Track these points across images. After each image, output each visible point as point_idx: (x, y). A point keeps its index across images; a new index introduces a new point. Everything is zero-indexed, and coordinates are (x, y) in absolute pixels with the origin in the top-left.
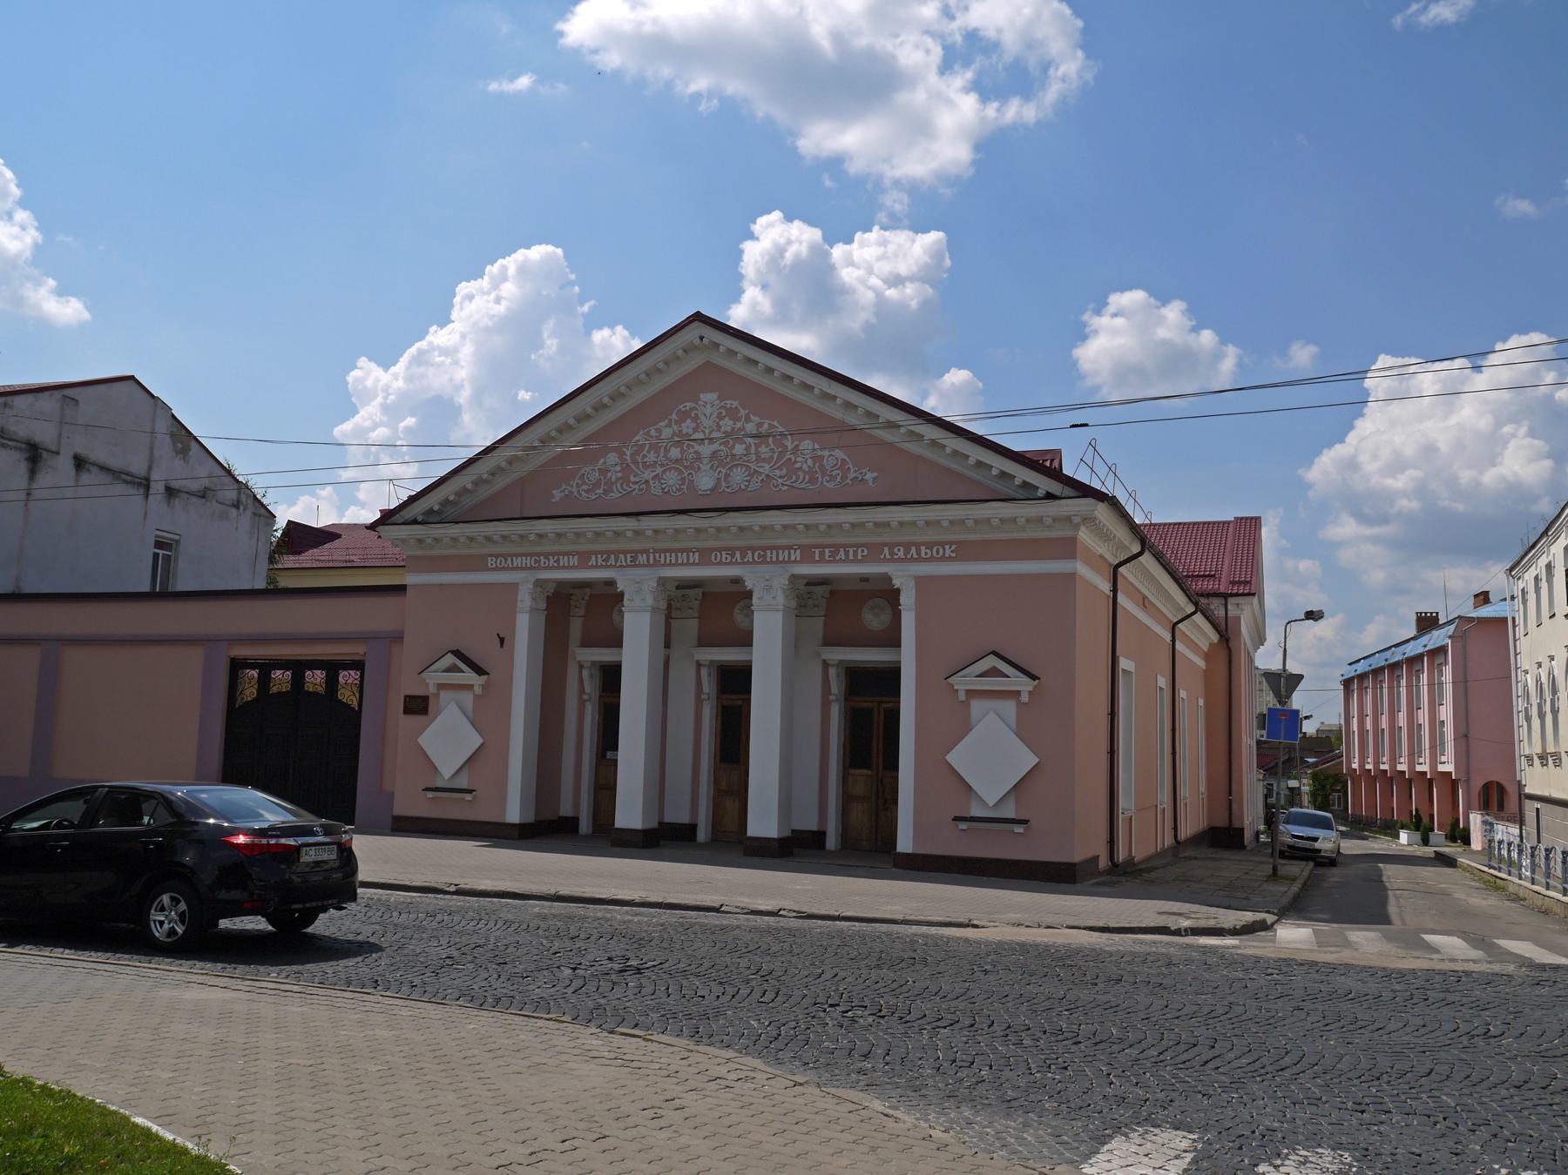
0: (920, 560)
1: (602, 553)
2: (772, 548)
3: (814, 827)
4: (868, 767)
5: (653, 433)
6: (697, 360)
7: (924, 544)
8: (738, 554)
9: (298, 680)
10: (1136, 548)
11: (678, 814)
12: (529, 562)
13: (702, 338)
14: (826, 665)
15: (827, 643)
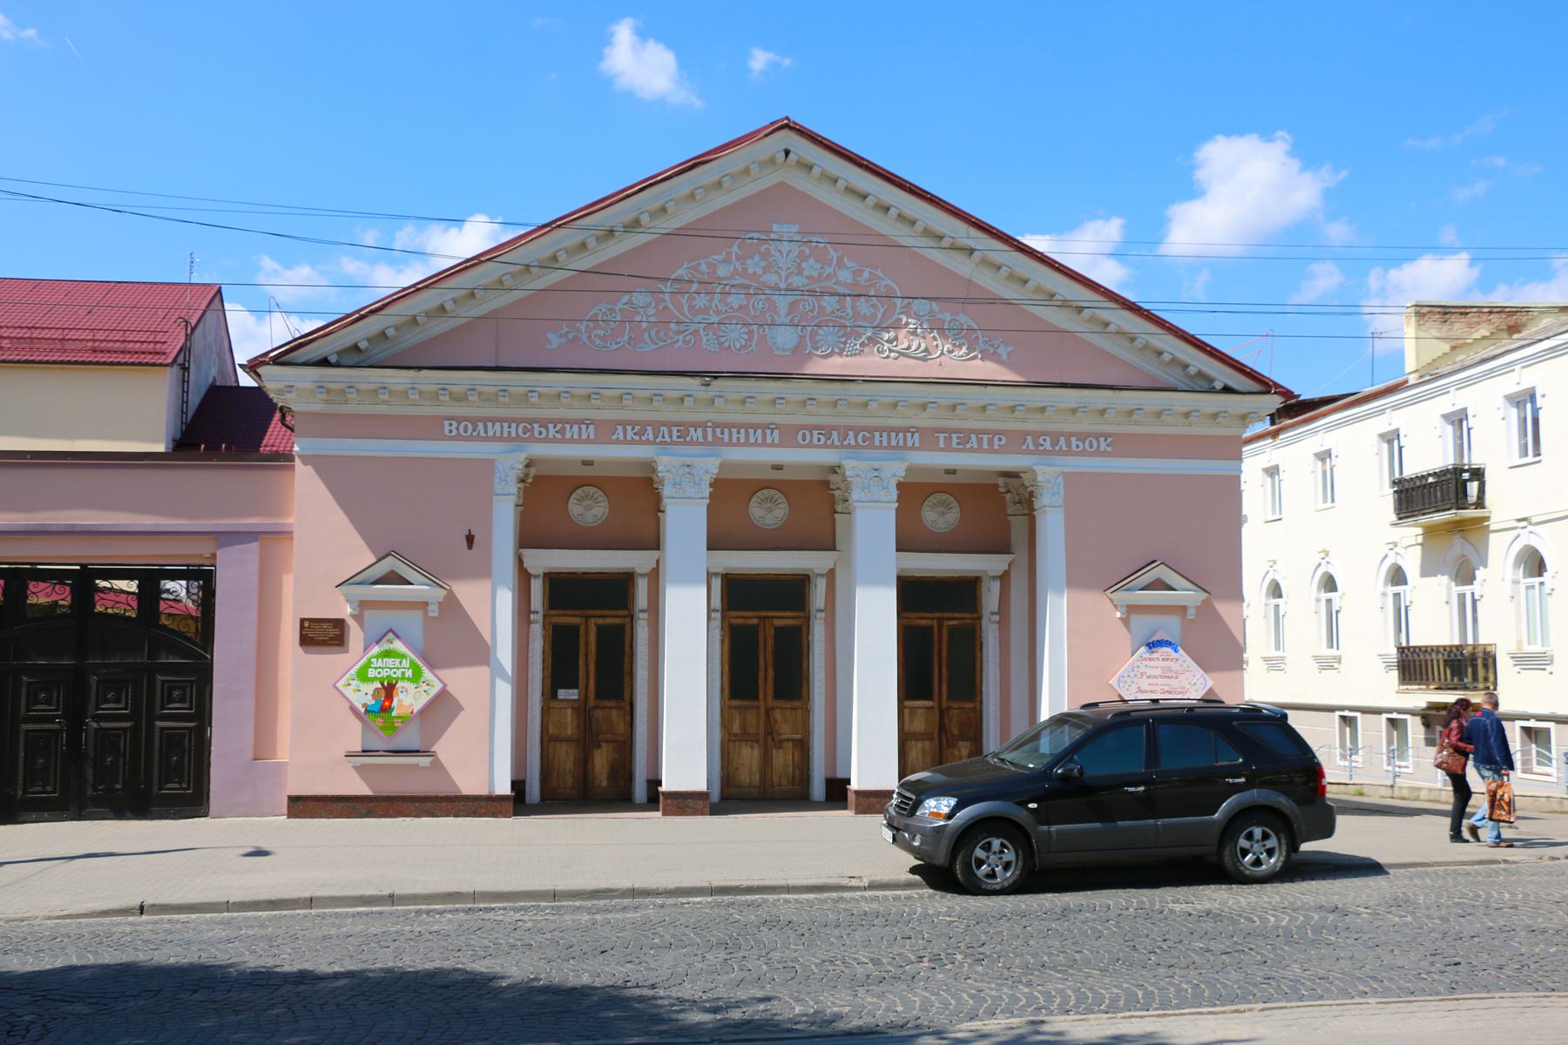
0: (1070, 453)
1: (633, 424)
2: (881, 430)
4: (928, 697)
5: (704, 268)
7: (1072, 434)
13: (787, 153)
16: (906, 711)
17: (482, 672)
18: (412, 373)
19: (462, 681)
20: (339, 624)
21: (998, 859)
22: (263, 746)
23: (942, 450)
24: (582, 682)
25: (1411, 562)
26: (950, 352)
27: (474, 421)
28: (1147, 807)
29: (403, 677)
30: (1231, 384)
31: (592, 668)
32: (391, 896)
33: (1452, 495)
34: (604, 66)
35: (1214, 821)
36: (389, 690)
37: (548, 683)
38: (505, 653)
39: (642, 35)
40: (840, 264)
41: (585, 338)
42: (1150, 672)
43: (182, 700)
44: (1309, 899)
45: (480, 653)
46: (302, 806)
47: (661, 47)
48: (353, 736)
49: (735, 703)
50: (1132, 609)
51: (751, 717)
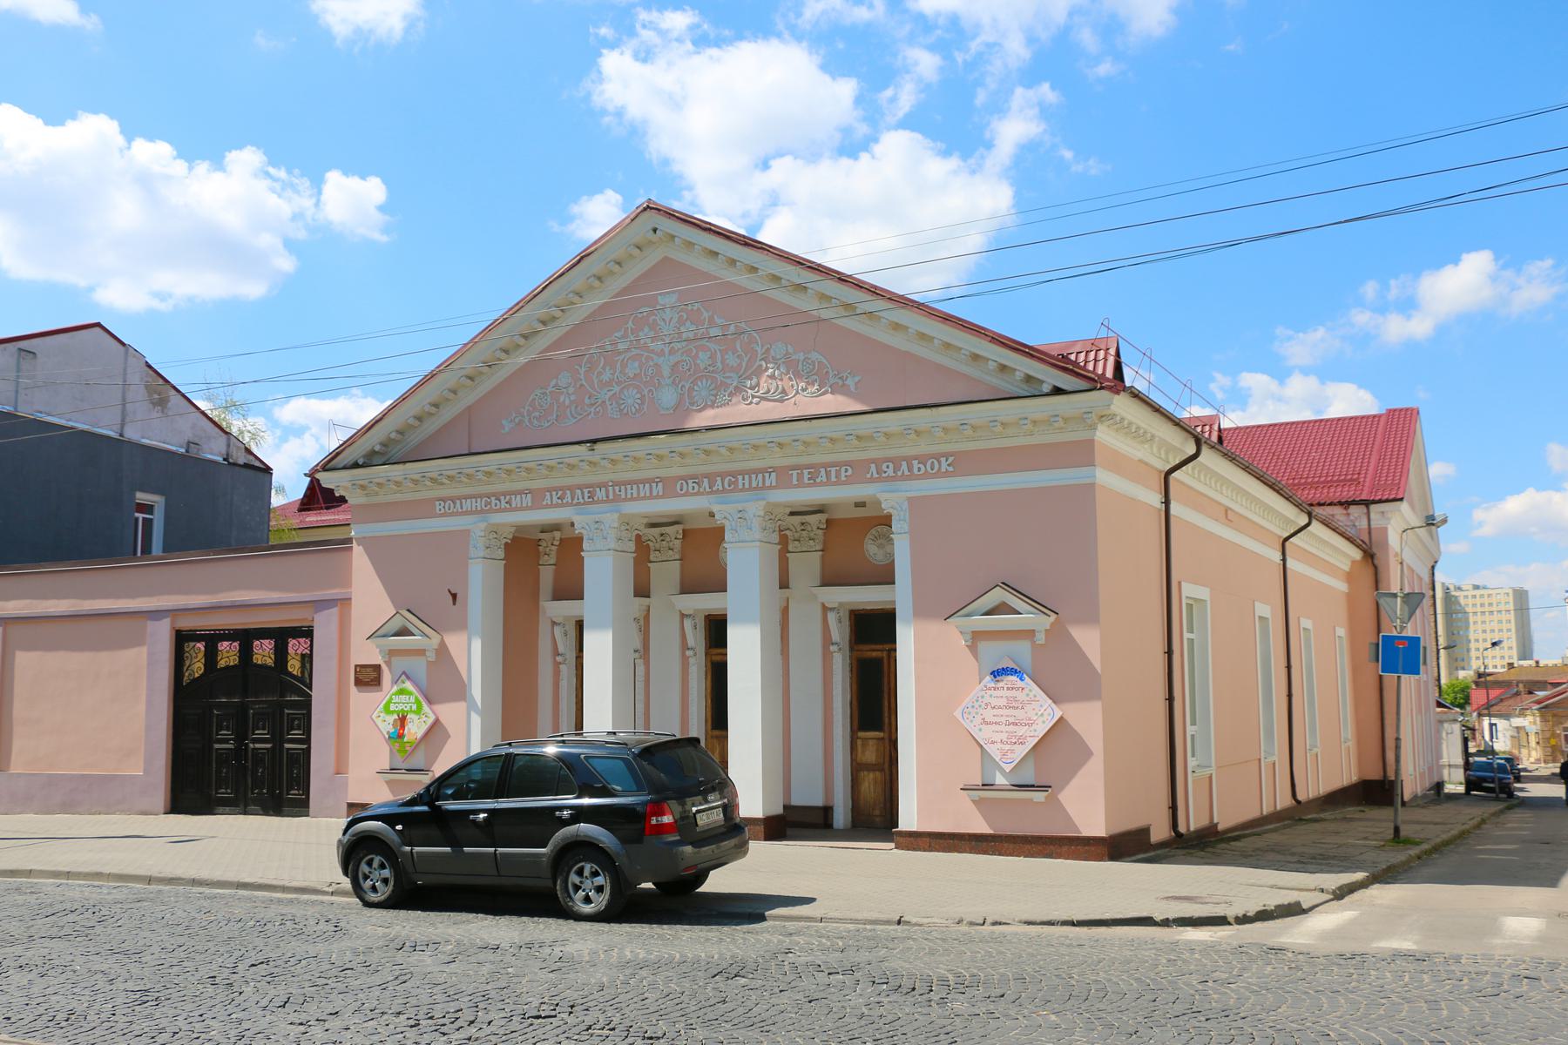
1: (556, 489)
2: (743, 473)
3: (818, 801)
4: (880, 729)
6: (653, 257)
9: (246, 652)
10: (1192, 450)
11: (808, 795)
12: (480, 504)
13: (655, 230)
15: (827, 582)
16: (859, 742)
17: (461, 706)
18: (400, 467)
19: (450, 713)
20: (377, 668)
21: (379, 877)
22: (340, 769)
26: (804, 390)
36: (402, 720)
38: (476, 691)
40: (711, 321)
42: (994, 702)
45: (459, 691)
50: (977, 637)
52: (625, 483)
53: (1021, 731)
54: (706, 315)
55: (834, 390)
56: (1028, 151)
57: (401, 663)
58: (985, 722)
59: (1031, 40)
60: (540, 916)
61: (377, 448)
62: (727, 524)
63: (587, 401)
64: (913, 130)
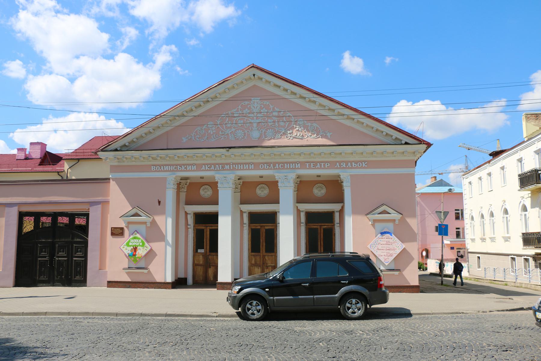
0: (352, 168)
1: (207, 164)
2: (287, 163)
6: (251, 84)
8: (349, 164)
13: (254, 75)
14: (242, 212)
17: (163, 243)
19: (157, 246)
20: (122, 229)
21: (255, 309)
22: (102, 266)
23: (308, 169)
24: (205, 247)
25: (528, 203)
26: (310, 136)
27: (160, 166)
28: (311, 290)
29: (139, 245)
30: (407, 141)
31: (208, 242)
32: (69, 313)
33: (535, 179)
34: (341, 66)
35: (336, 297)
36: (135, 249)
37: (195, 247)
38: (170, 237)
39: (353, 55)
41: (193, 139)
42: (382, 243)
43: (80, 252)
44: (298, 329)
45: (161, 237)
46: (112, 284)
47: (358, 58)
48: (125, 263)
49: (253, 254)
50: (375, 221)
51: (258, 258)
52: (238, 164)
53: (391, 252)
54: (271, 107)
55: (322, 137)
56: (166, 64)
57: (133, 227)
58: (378, 249)
59: (168, 29)
60: (318, 320)
61: (127, 144)
62: (280, 181)
63: (220, 133)
64: (128, 53)
